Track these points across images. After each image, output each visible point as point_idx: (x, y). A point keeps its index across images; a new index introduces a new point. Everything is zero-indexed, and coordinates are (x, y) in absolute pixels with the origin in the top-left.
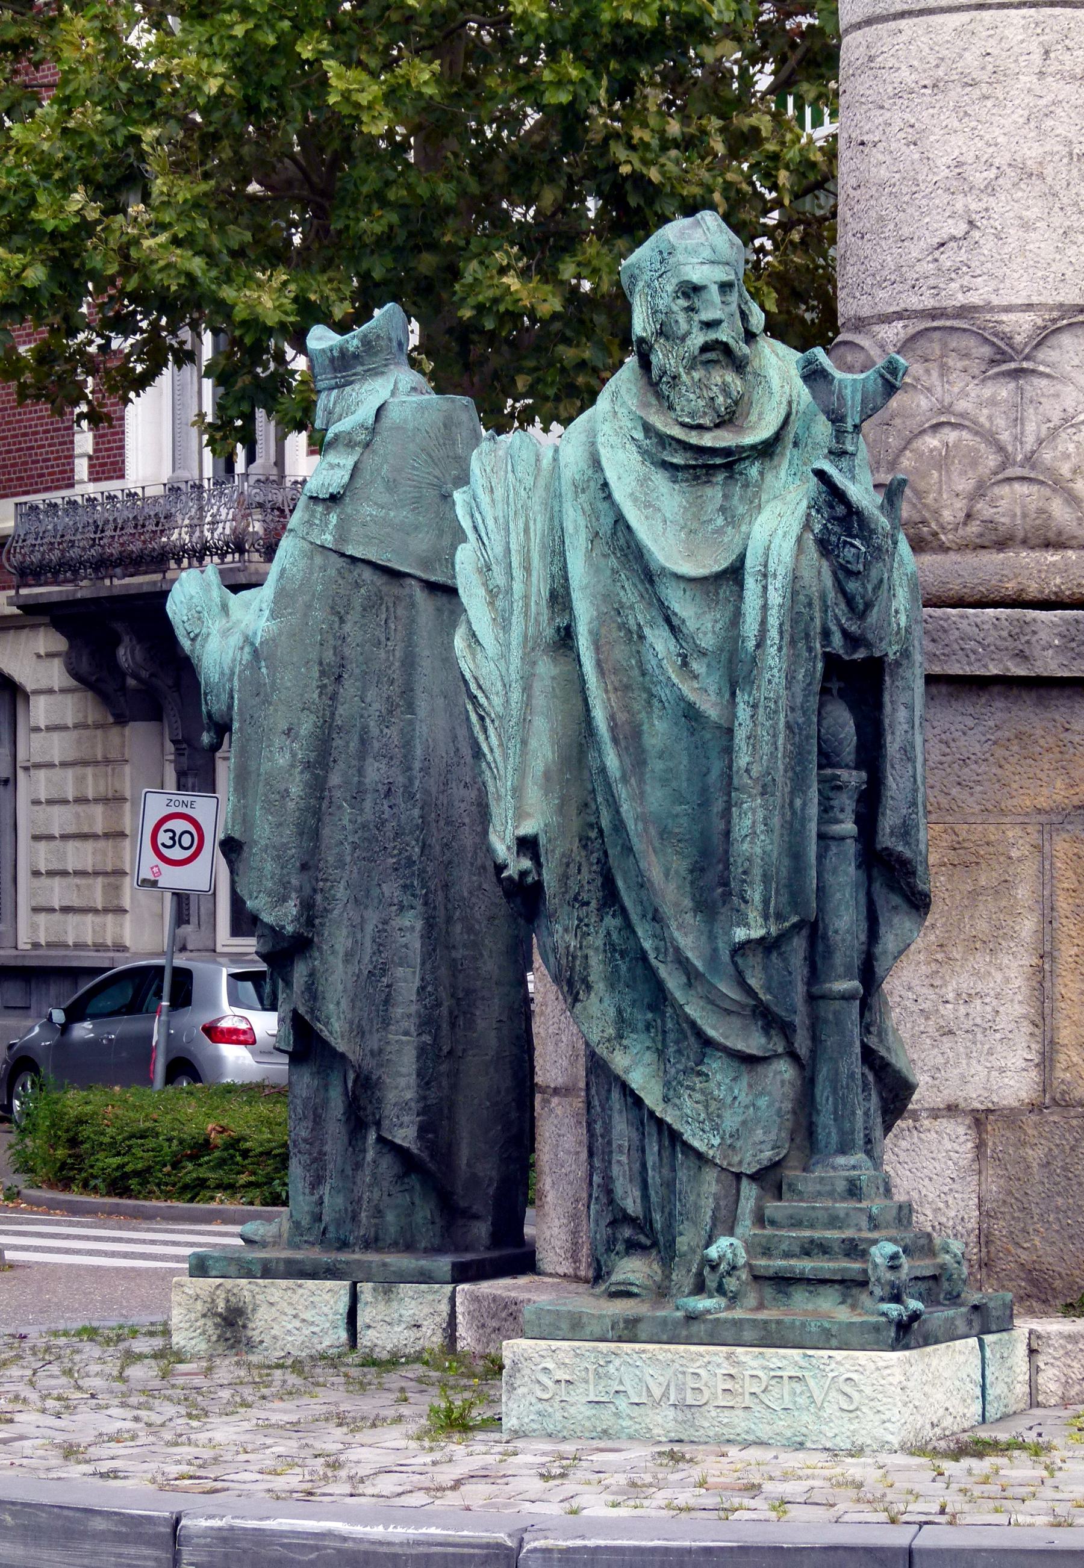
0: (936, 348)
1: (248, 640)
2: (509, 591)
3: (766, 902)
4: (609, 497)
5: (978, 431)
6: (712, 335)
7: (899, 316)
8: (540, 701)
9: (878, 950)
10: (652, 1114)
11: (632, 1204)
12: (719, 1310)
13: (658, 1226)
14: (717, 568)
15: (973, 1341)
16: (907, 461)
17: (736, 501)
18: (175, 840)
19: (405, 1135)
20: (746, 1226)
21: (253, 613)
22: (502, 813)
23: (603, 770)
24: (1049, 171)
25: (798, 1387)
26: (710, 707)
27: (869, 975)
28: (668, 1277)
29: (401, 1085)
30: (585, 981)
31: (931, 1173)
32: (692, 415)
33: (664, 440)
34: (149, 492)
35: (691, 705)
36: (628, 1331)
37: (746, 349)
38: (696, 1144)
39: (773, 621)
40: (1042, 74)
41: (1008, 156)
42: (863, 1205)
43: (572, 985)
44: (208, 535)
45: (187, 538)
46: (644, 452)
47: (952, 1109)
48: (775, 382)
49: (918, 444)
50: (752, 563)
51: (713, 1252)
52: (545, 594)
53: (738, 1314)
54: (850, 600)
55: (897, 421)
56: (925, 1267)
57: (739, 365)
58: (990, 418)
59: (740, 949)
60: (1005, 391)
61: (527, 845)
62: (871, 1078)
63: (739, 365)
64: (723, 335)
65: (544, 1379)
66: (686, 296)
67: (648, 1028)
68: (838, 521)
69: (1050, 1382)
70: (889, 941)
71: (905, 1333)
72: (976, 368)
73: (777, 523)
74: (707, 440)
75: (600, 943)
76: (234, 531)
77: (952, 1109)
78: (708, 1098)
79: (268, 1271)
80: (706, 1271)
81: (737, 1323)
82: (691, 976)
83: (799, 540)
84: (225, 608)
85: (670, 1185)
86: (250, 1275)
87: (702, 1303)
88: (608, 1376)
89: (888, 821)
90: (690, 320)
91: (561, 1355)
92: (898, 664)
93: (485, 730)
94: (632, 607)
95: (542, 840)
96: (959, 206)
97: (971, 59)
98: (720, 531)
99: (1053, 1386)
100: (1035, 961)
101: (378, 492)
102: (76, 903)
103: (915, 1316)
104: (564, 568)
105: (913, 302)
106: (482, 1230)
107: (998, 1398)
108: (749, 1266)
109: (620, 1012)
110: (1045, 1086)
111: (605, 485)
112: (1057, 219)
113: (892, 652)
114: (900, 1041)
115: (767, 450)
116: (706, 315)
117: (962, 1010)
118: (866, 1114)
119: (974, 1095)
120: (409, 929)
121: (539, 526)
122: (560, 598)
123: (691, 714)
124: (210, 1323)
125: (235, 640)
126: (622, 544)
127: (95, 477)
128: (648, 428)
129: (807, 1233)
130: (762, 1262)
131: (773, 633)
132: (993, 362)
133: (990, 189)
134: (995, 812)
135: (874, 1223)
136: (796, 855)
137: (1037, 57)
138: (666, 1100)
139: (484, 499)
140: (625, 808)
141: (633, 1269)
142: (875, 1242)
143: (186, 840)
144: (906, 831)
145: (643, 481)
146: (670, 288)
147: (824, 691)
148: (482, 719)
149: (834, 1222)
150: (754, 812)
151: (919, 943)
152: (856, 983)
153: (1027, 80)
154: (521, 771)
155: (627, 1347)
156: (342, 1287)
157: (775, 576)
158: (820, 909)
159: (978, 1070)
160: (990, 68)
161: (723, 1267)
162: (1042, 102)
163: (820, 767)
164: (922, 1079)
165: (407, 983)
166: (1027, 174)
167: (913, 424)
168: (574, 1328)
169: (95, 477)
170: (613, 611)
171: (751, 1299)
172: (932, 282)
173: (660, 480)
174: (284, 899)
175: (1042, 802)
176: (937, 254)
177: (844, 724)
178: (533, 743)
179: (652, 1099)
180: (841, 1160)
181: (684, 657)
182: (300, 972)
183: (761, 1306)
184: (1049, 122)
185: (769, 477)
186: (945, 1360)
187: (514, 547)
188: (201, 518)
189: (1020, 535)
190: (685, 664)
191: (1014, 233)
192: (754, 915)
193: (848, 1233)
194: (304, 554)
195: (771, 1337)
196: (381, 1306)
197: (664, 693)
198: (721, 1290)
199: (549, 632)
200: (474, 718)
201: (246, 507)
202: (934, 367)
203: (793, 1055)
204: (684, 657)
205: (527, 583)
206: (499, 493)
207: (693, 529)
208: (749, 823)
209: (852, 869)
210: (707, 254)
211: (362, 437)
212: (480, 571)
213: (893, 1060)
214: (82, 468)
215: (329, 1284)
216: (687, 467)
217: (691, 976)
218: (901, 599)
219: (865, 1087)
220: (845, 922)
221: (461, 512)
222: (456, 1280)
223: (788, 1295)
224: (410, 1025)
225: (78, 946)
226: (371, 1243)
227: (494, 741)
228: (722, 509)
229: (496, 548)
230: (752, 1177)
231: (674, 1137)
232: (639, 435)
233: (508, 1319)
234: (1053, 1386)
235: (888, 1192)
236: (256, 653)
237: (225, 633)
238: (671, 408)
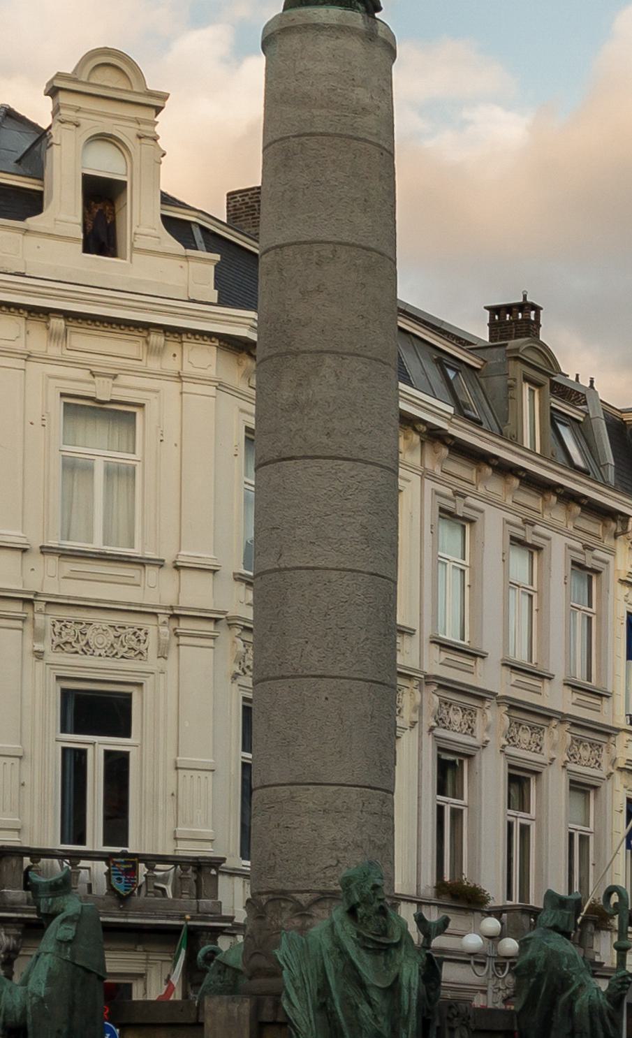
0: (328, 905)
7: (308, 891)
24: (364, 845)
33: (365, 939)
40: (362, 811)
41: (351, 839)
46: (355, 942)
52: (316, 990)
54: (430, 1000)
90: (374, 898)
94: (353, 997)
96: (334, 855)
97: (339, 803)
105: (315, 887)
133: (345, 849)
146: (370, 886)
157: (414, 989)
160: (345, 807)
162: (363, 821)
170: (345, 999)
172: (323, 881)
173: (362, 952)
176: (324, 871)
181: (375, 1016)
204: (375, 1016)
216: (374, 949)
229: (296, 972)
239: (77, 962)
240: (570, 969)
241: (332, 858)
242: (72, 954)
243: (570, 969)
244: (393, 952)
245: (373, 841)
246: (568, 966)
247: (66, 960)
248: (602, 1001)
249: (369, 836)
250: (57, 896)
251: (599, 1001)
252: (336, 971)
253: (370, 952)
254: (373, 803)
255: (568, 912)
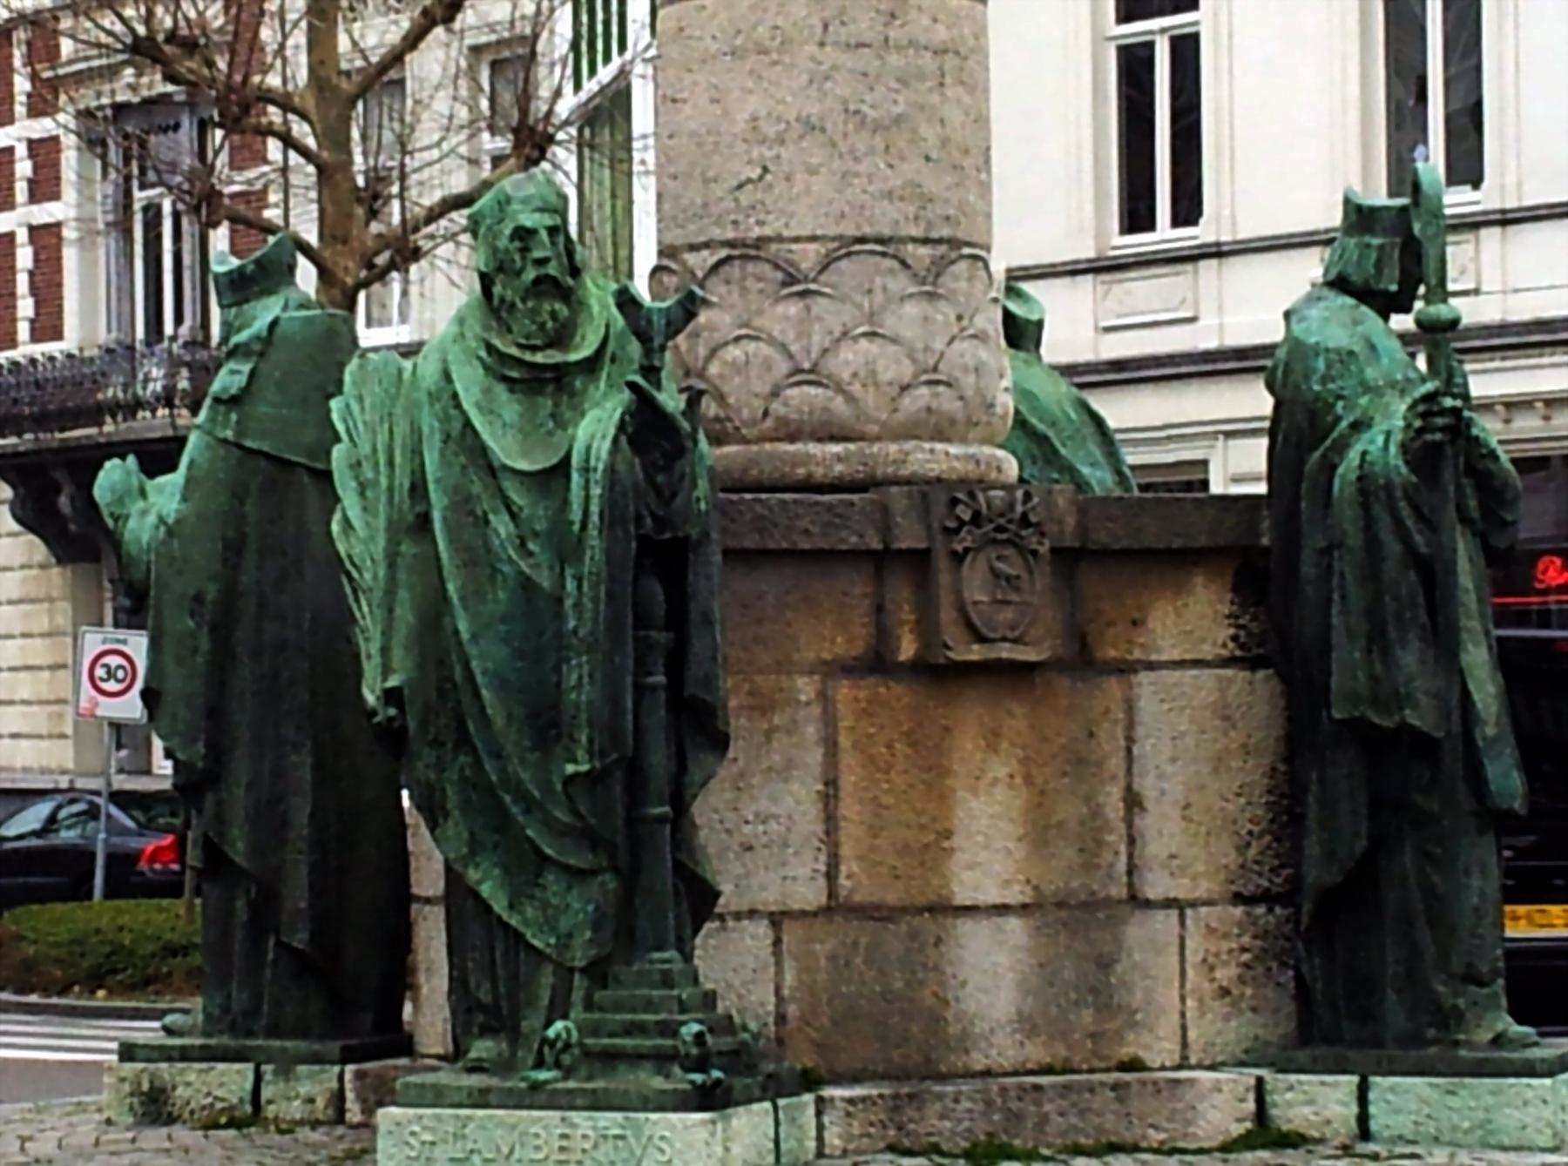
1: (161, 520)
2: (376, 482)
3: (591, 741)
4: (458, 406)
5: (771, 341)
6: (542, 271)
7: (706, 245)
8: (402, 576)
9: (687, 779)
10: (499, 918)
11: (484, 995)
12: (556, 1080)
13: (505, 1011)
14: (547, 464)
15: (767, 1105)
16: (713, 369)
17: (564, 407)
18: (111, 674)
19: (300, 940)
20: (577, 1012)
21: (166, 495)
22: (371, 668)
23: (456, 632)
24: (829, 126)
25: (620, 1143)
26: (545, 580)
27: (680, 803)
28: (513, 1053)
29: (297, 895)
30: (443, 808)
31: (738, 969)
32: (527, 337)
33: (503, 358)
34: (87, 354)
35: (528, 579)
36: (480, 1099)
37: (570, 281)
38: (536, 943)
39: (594, 508)
40: (822, 44)
42: (675, 992)
43: (432, 812)
44: (140, 392)
45: (120, 395)
46: (486, 368)
47: (752, 913)
48: (596, 309)
49: (721, 353)
50: (575, 460)
51: (551, 1033)
52: (407, 484)
53: (571, 1084)
54: (657, 490)
55: (705, 334)
56: (726, 1043)
57: (566, 295)
58: (783, 332)
59: (569, 780)
60: (793, 308)
61: (391, 696)
62: (681, 887)
63: (566, 295)
64: (552, 270)
65: (412, 1141)
66: (521, 239)
67: (496, 846)
68: (648, 429)
69: (833, 1139)
70: (695, 774)
71: (710, 1099)
72: (770, 289)
73: (597, 425)
74: (539, 358)
75: (455, 777)
76: (165, 387)
77: (752, 913)
78: (545, 906)
79: (185, 1055)
80: (546, 1050)
81: (569, 1091)
82: (530, 805)
83: (615, 441)
84: (143, 494)
85: (514, 977)
86: (170, 1059)
87: (543, 1075)
88: (464, 1137)
89: (694, 671)
90: (523, 258)
91: (425, 1122)
92: (699, 543)
93: (357, 600)
95: (406, 692)
96: (755, 154)
98: (550, 433)
99: (837, 1142)
100: (820, 787)
101: (270, 393)
102: (25, 730)
103: (718, 1082)
104: (422, 464)
105: (717, 233)
106: (367, 1019)
107: (790, 1151)
108: (581, 1044)
109: (472, 834)
110: (832, 894)
111: (455, 396)
112: (837, 164)
113: (694, 533)
114: (707, 856)
115: (591, 366)
116: (538, 254)
117: (761, 828)
118: (677, 917)
119: (769, 898)
120: (302, 766)
121: (402, 429)
122: (418, 489)
123: (527, 585)
124: (135, 1100)
125: (151, 519)
126: (467, 444)
127: (36, 337)
128: (490, 348)
129: (628, 1017)
130: (589, 1041)
131: (595, 518)
132: (785, 284)
134: (785, 667)
135: (683, 1008)
136: (615, 702)
137: (819, 30)
138: (511, 907)
139: (355, 407)
140: (474, 664)
141: (481, 1049)
142: (684, 1023)
143: (120, 674)
144: (709, 681)
145: (487, 391)
146: (507, 232)
147: (639, 567)
148: (355, 591)
149: (650, 1005)
150: (580, 666)
151: (722, 773)
152: (666, 809)
153: (811, 48)
154: (387, 633)
155: (480, 1113)
156: (250, 1066)
158: (637, 748)
159: (774, 878)
161: (559, 1045)
163: (636, 628)
164: (726, 888)
165: (301, 811)
166: (810, 127)
167: (717, 337)
168: (437, 1097)
169: (36, 337)
170: (462, 503)
171: (583, 1072)
173: (500, 390)
174: (194, 740)
175: (826, 656)
177: (656, 592)
178: (398, 611)
179: (499, 906)
180: (657, 955)
182: (209, 800)
183: (590, 1078)
184: (829, 85)
185: (592, 388)
186: (744, 1120)
187: (380, 447)
188: (134, 376)
189: (807, 429)
190: (523, 544)
191: (800, 177)
192: (581, 754)
193: (662, 1016)
194: (208, 447)
195: (598, 1103)
196: (281, 1085)
197: (506, 568)
198: (557, 1065)
199: (410, 518)
200: (348, 590)
201: (174, 364)
202: (735, 289)
203: (615, 870)
205: (391, 477)
206: (367, 402)
207: (528, 431)
208: (574, 677)
209: (663, 713)
210: (538, 203)
211: (257, 347)
212: (351, 467)
213: (699, 870)
214: (23, 330)
215: (236, 1066)
217: (530, 805)
218: (703, 486)
219: (677, 893)
220: (659, 759)
221: (335, 416)
222: (344, 1061)
223: (614, 1069)
224: (303, 846)
225: (25, 770)
226: (274, 1031)
227: (365, 609)
228: (553, 416)
229: (365, 448)
230: (583, 970)
231: (519, 936)
232: (483, 354)
233: (379, 1094)
234: (837, 1142)
235: (696, 981)
236: (170, 532)
237: (144, 513)
238: (510, 331)
239: (249, 443)
240: (1331, 386)
241: (749, 162)
242: (241, 430)
243: (1331, 386)
244: (578, 384)
245: (857, 112)
246: (1325, 380)
247: (225, 441)
248: (1393, 462)
249: (845, 102)
250: (247, 301)
251: (1387, 464)
252: (447, 438)
253: (518, 387)
254: (854, 21)
255: (1376, 241)
